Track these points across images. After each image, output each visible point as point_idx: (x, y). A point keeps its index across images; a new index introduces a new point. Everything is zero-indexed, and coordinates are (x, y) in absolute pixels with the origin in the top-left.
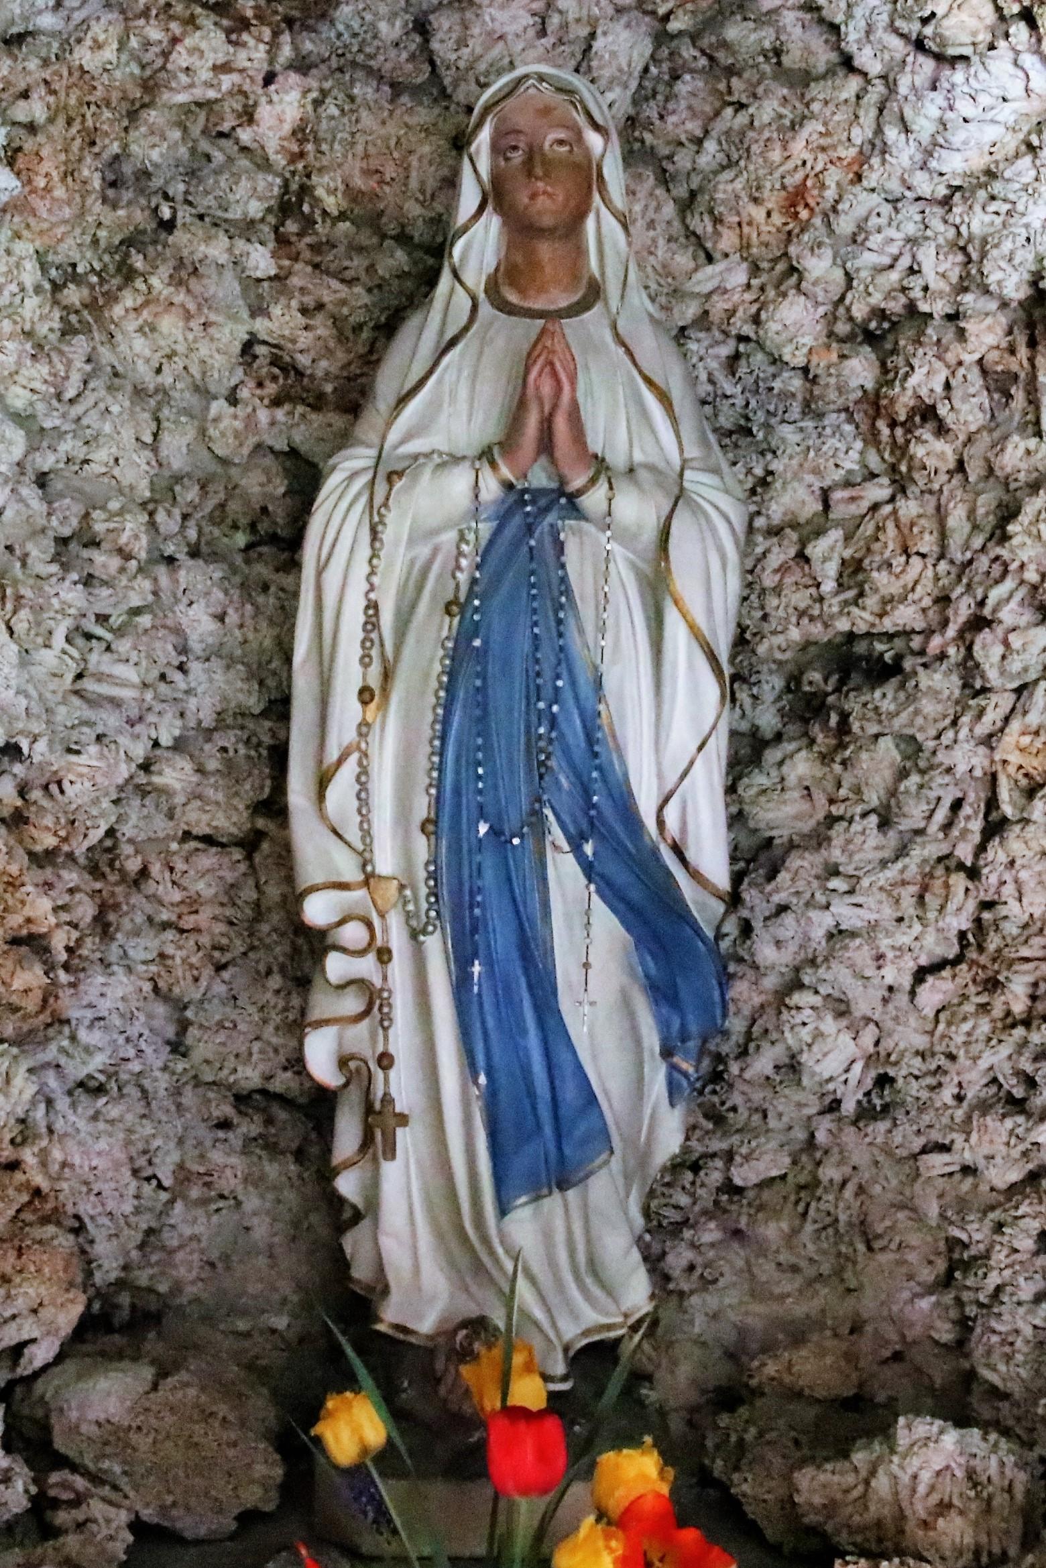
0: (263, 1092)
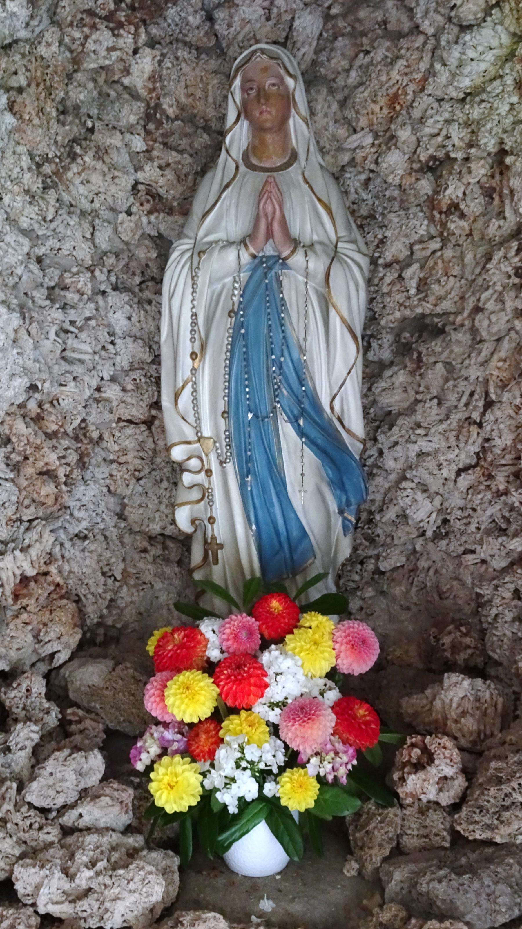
0: (162, 535)
